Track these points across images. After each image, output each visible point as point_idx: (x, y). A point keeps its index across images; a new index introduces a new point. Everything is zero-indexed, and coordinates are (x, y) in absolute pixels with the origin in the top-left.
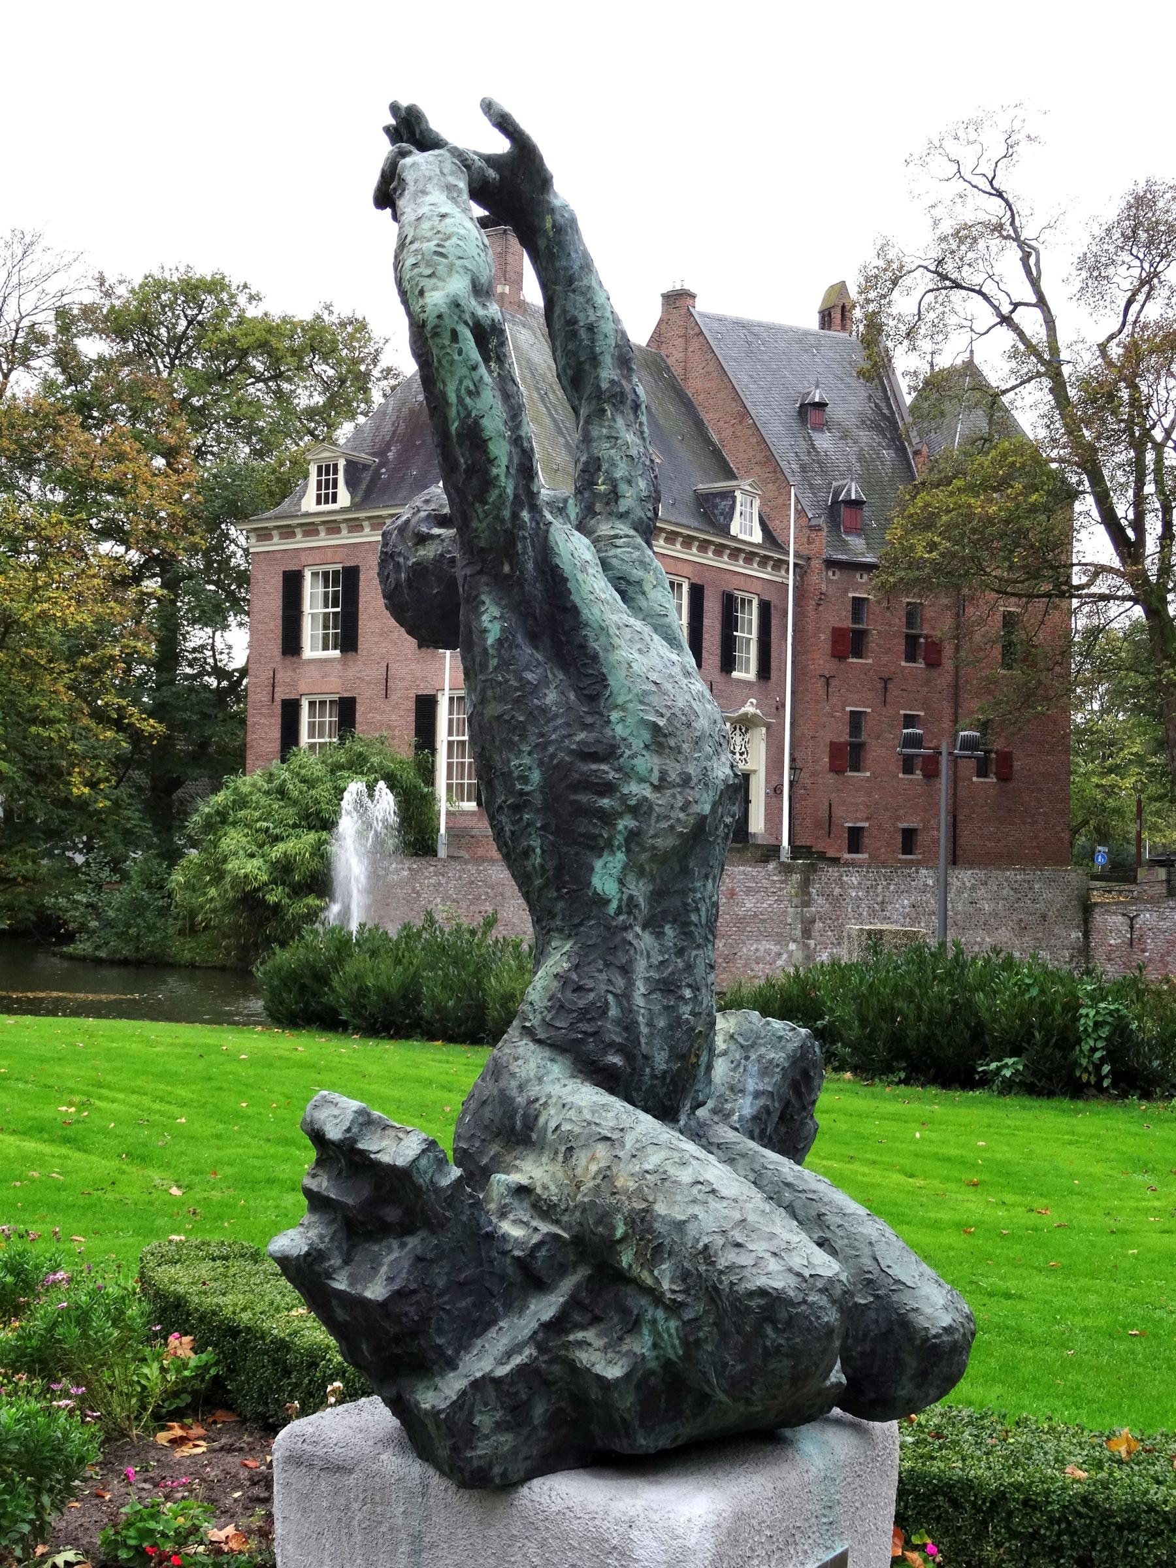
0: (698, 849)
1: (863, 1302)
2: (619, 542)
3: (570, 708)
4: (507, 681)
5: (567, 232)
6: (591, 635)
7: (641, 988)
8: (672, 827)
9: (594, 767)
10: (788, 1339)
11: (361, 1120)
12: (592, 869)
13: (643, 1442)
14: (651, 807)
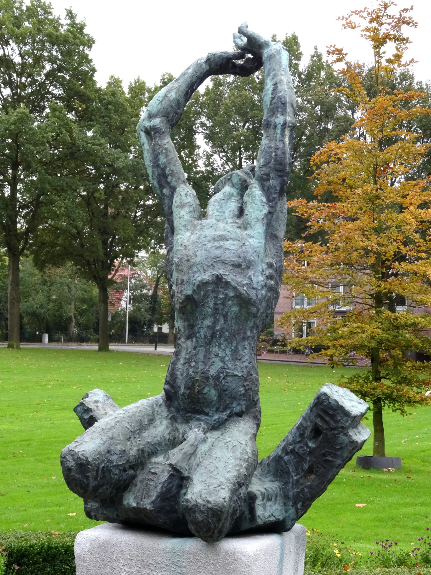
7: (182, 361)
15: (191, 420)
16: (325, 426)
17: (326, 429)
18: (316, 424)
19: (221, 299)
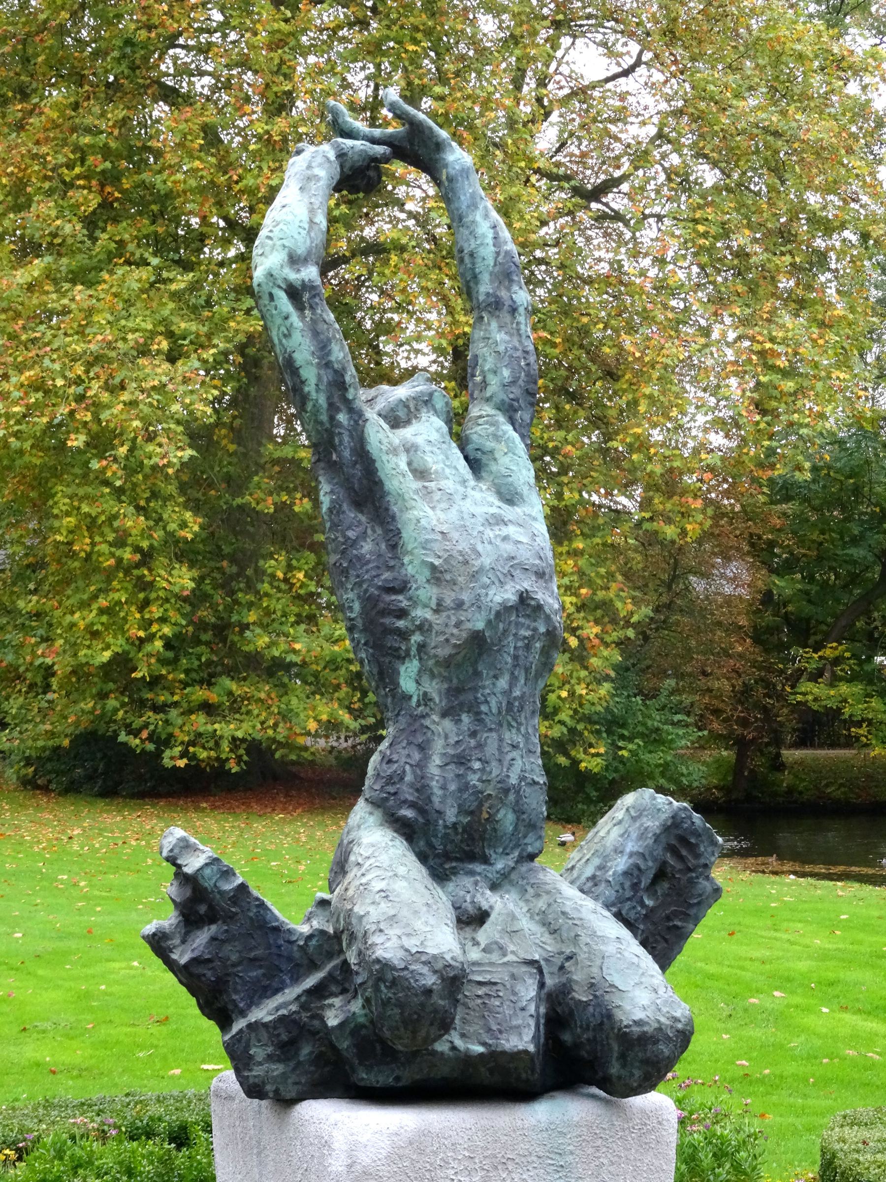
0: (485, 656)
1: (584, 999)
2: (481, 421)
3: (380, 556)
4: (337, 538)
5: (457, 181)
6: (392, 500)
7: (437, 760)
8: (447, 640)
9: (394, 597)
10: (394, 994)
11: (181, 844)
12: (399, 673)
13: (365, 1076)
14: (430, 625)
15: (455, 874)
16: (679, 866)
17: (680, 871)
18: (664, 863)
19: (525, 638)
